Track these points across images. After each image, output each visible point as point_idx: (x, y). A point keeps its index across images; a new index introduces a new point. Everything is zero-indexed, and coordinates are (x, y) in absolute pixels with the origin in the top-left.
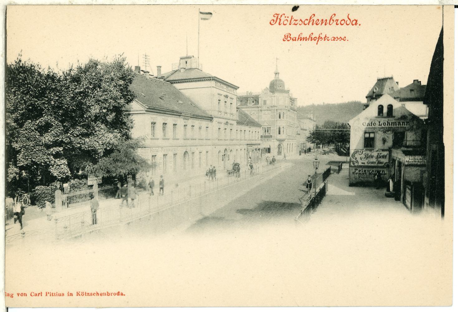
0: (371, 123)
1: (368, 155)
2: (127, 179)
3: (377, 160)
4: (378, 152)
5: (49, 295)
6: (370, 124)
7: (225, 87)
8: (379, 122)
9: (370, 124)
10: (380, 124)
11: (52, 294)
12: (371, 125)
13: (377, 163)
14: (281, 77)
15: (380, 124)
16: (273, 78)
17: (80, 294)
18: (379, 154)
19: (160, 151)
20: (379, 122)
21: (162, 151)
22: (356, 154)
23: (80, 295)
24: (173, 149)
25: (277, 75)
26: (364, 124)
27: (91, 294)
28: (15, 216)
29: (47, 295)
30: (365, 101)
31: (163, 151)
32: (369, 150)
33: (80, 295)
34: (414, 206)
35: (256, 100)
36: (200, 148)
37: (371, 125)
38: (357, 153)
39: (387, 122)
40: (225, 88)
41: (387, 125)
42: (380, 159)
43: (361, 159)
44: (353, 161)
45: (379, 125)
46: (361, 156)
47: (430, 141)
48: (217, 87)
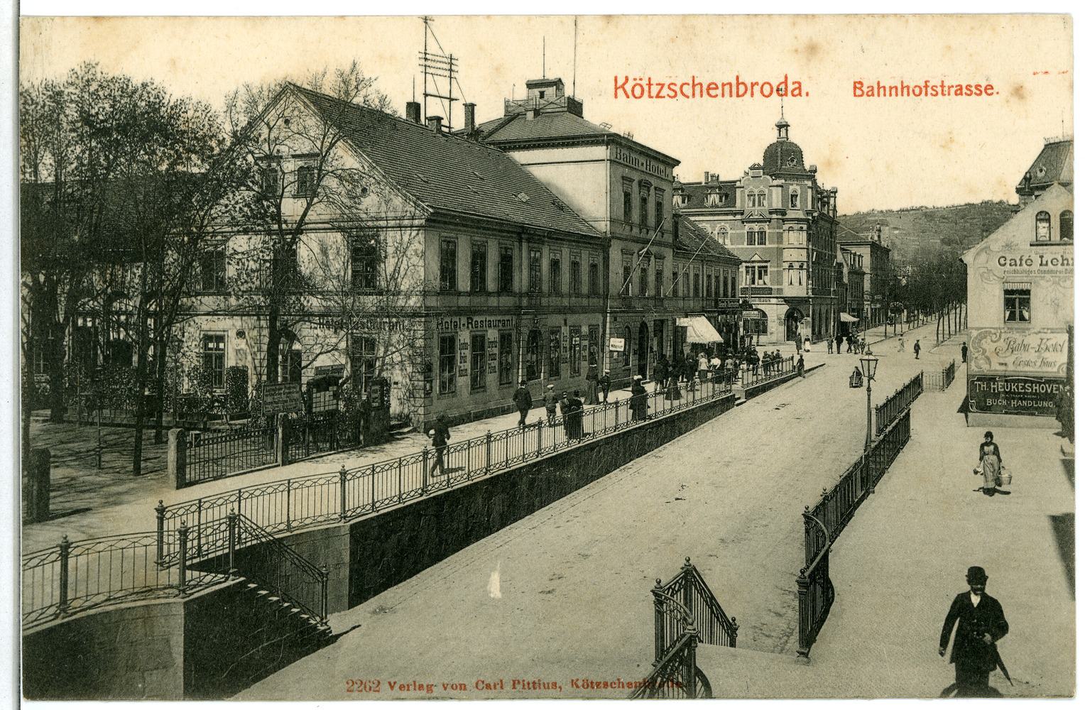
0: (1021, 260)
1: (1015, 342)
2: (48, 474)
3: (1039, 357)
4: (1043, 335)
5: (519, 687)
6: (1018, 263)
7: (642, 160)
8: (1042, 257)
9: (1018, 263)
10: (1044, 262)
11: (529, 684)
12: (1021, 265)
13: (1038, 364)
14: (795, 136)
15: (1044, 262)
16: (772, 137)
17: (580, 683)
18: (1044, 341)
19: (464, 325)
20: (1042, 257)
21: (468, 327)
22: (983, 341)
23: (577, 687)
24: (499, 321)
25: (783, 130)
26: (1002, 261)
27: (606, 685)
28: (717, 359)
29: (516, 686)
30: (1014, 199)
31: (470, 326)
32: (1016, 329)
33: (577, 687)
34: (24, 696)
35: (727, 190)
36: (572, 319)
37: (1021, 265)
38: (985, 337)
39: (1062, 256)
40: (642, 164)
41: (1063, 264)
42: (1047, 355)
43: (997, 354)
44: (976, 358)
45: (1041, 265)
46: (995, 345)
47: (644, 419)
48: (621, 161)
